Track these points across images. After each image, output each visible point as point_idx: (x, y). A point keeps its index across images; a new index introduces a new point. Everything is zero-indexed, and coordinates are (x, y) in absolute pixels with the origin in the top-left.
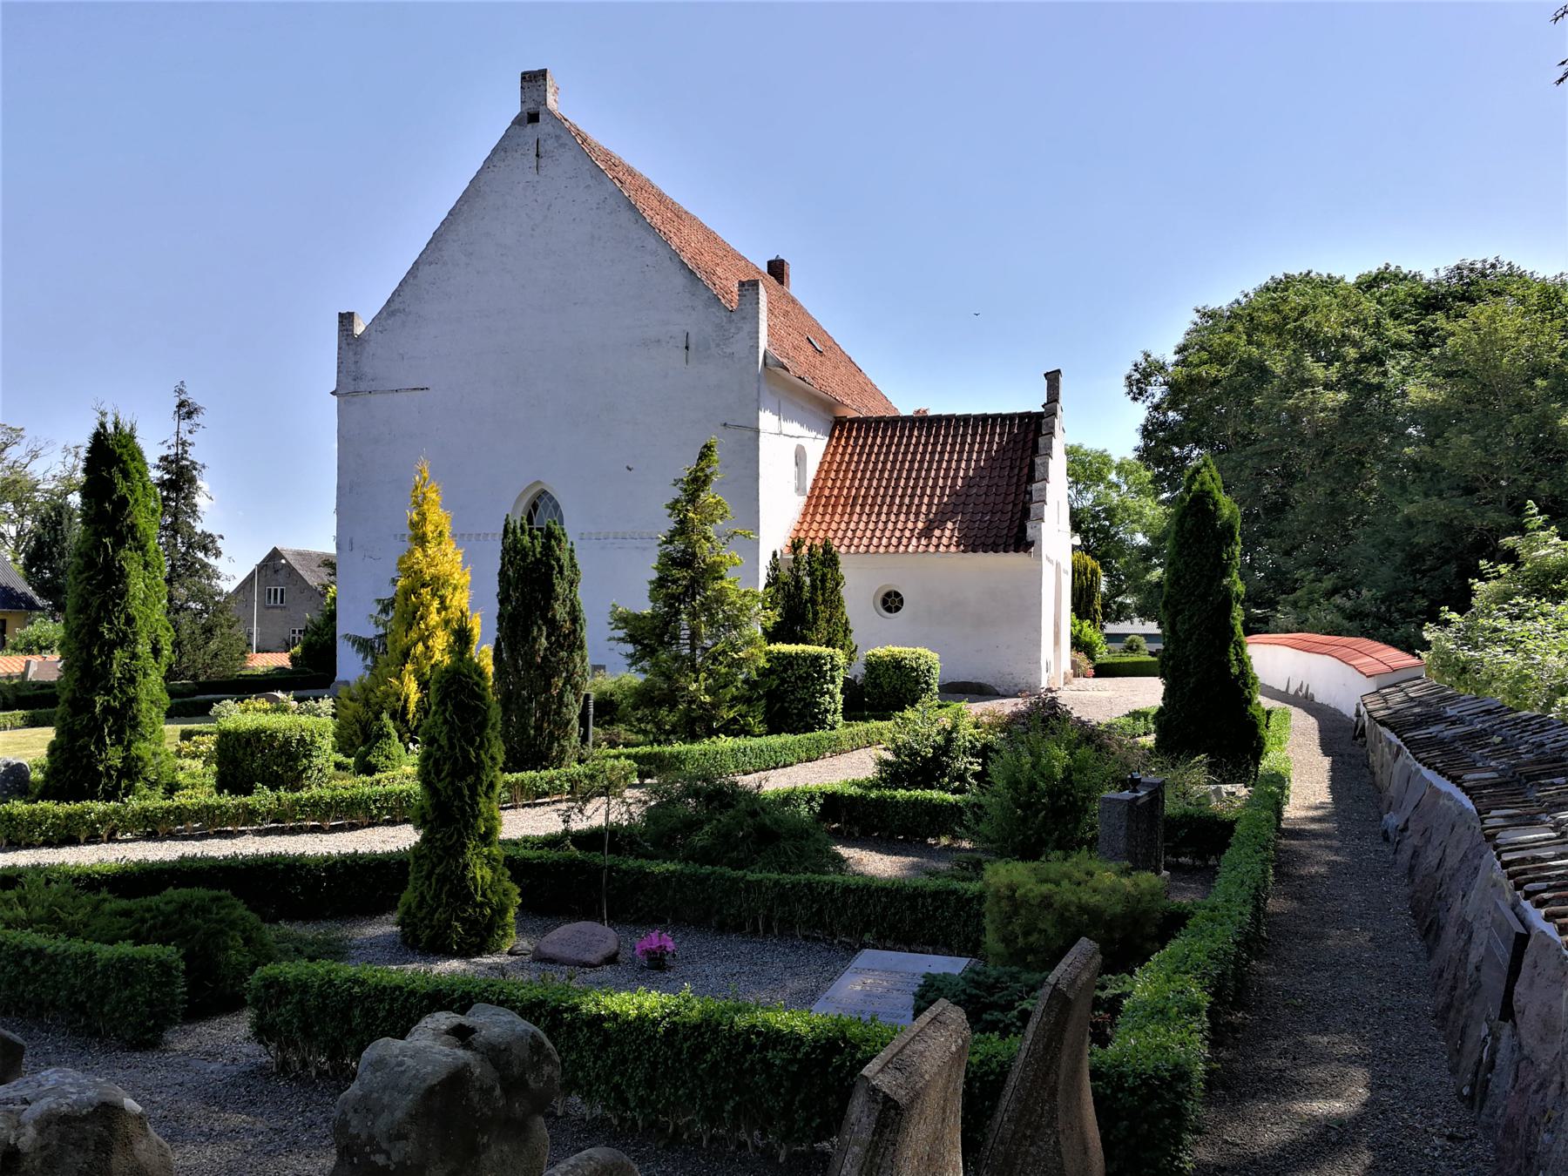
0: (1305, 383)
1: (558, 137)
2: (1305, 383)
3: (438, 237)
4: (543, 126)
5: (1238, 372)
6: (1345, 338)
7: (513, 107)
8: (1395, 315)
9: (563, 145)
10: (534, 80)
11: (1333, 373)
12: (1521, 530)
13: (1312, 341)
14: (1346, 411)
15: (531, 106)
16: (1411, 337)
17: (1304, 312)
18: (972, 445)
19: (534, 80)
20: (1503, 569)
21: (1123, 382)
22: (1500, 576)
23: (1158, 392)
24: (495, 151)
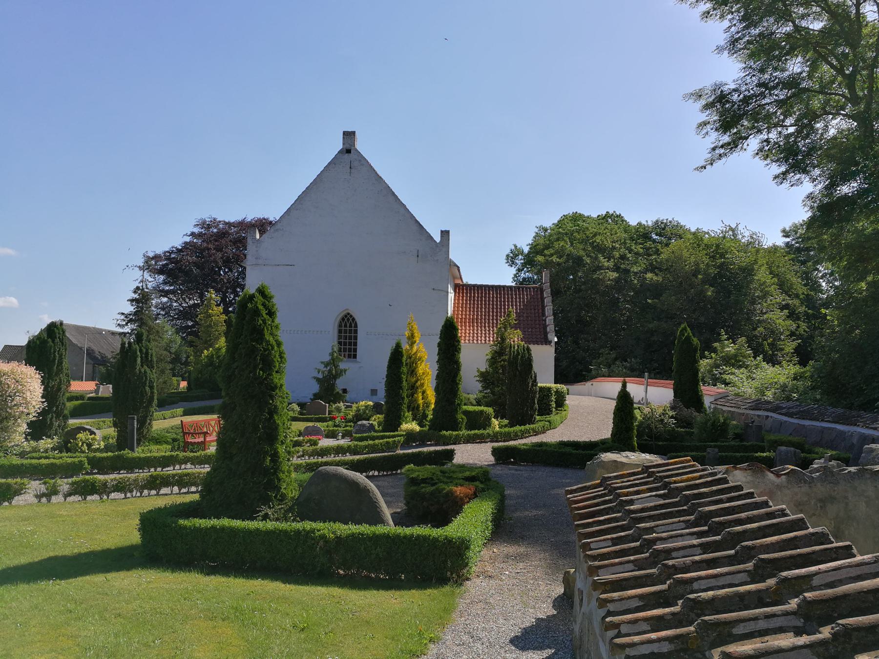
0: (600, 268)
1: (360, 161)
2: (600, 268)
3: (300, 198)
4: (352, 155)
5: (567, 261)
6: (614, 248)
7: (339, 145)
8: (632, 239)
9: (363, 165)
10: (349, 136)
11: (611, 264)
12: (719, 341)
13: (600, 249)
14: (617, 280)
15: (348, 146)
16: (641, 250)
17: (595, 235)
18: (516, 298)
19: (349, 136)
20: (713, 355)
21: (505, 257)
22: (711, 358)
23: (519, 261)
24: (330, 164)
